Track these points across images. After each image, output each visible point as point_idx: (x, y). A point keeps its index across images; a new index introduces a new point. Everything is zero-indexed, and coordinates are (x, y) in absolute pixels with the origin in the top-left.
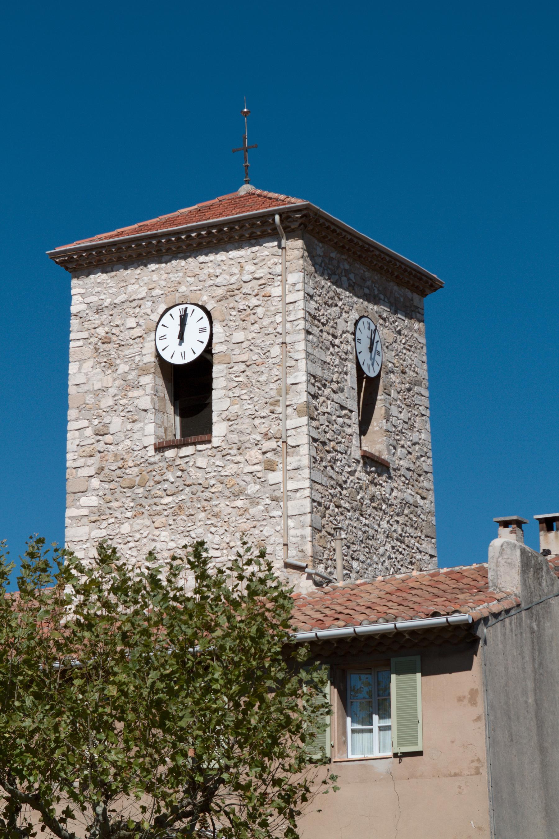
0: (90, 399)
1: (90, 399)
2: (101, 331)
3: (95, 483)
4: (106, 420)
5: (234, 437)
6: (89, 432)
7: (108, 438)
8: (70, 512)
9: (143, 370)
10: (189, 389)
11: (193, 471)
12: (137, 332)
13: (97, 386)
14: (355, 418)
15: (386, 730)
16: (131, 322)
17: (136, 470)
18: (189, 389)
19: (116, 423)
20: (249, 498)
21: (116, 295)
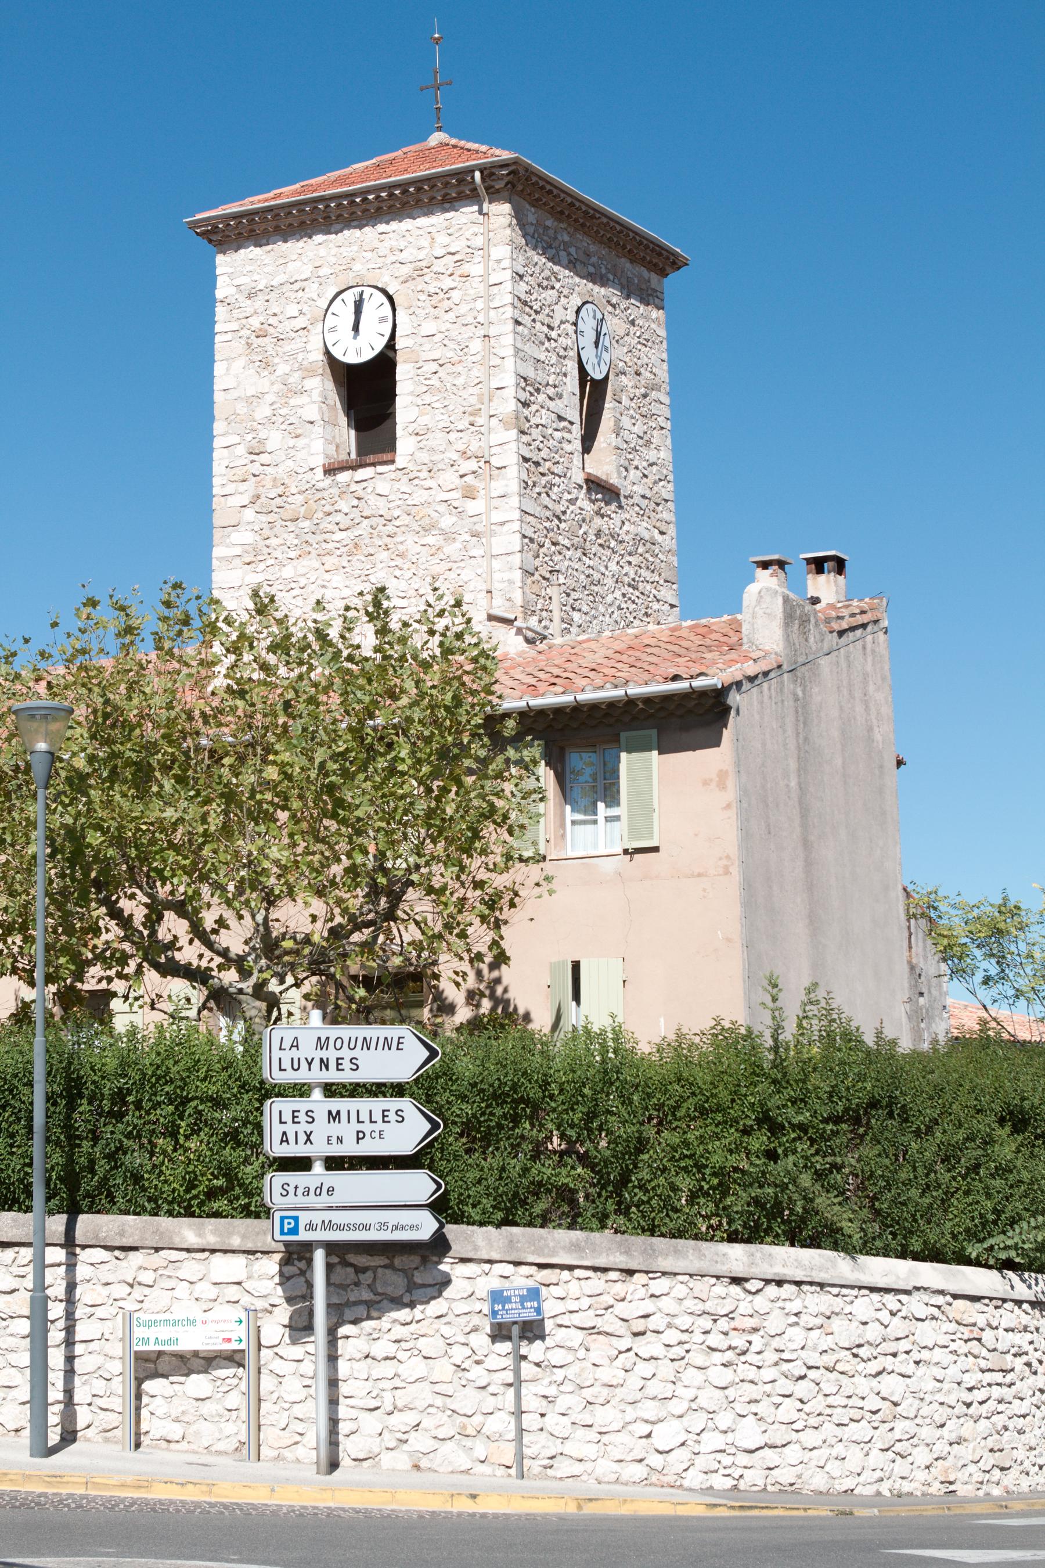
0: (241, 408)
1: (241, 408)
2: (255, 322)
3: (249, 514)
4: (262, 435)
6: (241, 450)
7: (264, 458)
16: (292, 310)
17: (300, 499)
18: (367, 393)
19: (275, 439)
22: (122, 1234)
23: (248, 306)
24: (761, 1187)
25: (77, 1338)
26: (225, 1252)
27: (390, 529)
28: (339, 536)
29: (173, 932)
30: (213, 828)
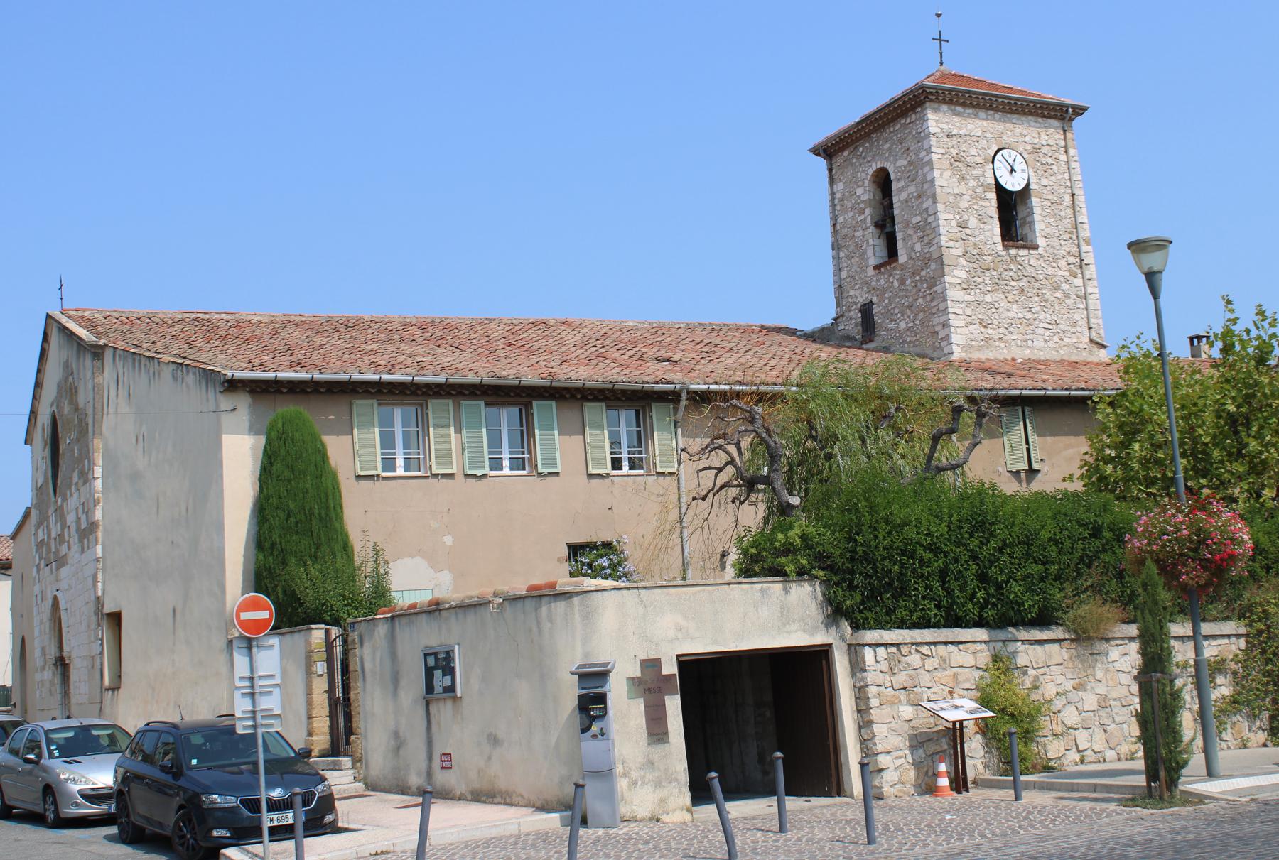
0: (952, 199)
1: (952, 199)
2: (954, 152)
3: (962, 261)
4: (965, 217)
5: (1051, 250)
6: (954, 223)
7: (967, 231)
8: (947, 279)
9: (987, 188)
10: (1011, 209)
11: (1028, 268)
12: (979, 160)
13: (956, 191)
14: (62, 605)
15: (347, 666)
16: (973, 152)
17: (990, 258)
18: (1011, 209)
19: (973, 222)
20: (1063, 292)
21: (960, 128)
22: (882, 637)
23: (949, 142)
24: (184, 836)
25: (879, 748)
26: (792, 332)
27: (1037, 285)
28: (1013, 284)
29: (372, 539)
30: (901, 708)
